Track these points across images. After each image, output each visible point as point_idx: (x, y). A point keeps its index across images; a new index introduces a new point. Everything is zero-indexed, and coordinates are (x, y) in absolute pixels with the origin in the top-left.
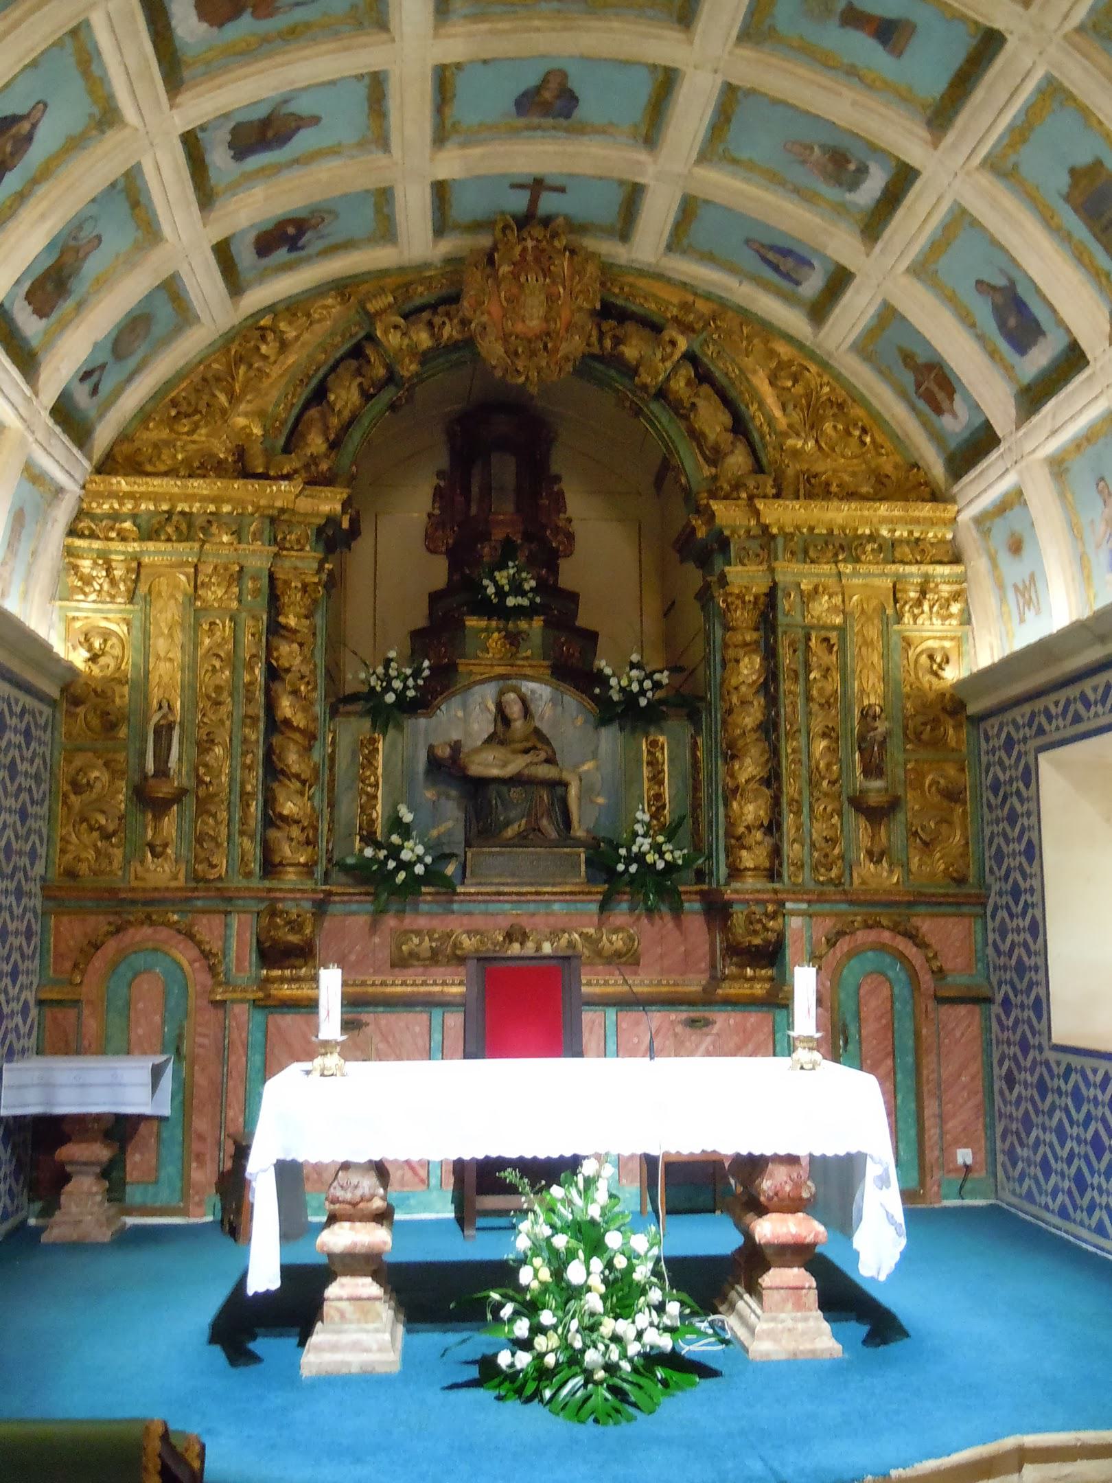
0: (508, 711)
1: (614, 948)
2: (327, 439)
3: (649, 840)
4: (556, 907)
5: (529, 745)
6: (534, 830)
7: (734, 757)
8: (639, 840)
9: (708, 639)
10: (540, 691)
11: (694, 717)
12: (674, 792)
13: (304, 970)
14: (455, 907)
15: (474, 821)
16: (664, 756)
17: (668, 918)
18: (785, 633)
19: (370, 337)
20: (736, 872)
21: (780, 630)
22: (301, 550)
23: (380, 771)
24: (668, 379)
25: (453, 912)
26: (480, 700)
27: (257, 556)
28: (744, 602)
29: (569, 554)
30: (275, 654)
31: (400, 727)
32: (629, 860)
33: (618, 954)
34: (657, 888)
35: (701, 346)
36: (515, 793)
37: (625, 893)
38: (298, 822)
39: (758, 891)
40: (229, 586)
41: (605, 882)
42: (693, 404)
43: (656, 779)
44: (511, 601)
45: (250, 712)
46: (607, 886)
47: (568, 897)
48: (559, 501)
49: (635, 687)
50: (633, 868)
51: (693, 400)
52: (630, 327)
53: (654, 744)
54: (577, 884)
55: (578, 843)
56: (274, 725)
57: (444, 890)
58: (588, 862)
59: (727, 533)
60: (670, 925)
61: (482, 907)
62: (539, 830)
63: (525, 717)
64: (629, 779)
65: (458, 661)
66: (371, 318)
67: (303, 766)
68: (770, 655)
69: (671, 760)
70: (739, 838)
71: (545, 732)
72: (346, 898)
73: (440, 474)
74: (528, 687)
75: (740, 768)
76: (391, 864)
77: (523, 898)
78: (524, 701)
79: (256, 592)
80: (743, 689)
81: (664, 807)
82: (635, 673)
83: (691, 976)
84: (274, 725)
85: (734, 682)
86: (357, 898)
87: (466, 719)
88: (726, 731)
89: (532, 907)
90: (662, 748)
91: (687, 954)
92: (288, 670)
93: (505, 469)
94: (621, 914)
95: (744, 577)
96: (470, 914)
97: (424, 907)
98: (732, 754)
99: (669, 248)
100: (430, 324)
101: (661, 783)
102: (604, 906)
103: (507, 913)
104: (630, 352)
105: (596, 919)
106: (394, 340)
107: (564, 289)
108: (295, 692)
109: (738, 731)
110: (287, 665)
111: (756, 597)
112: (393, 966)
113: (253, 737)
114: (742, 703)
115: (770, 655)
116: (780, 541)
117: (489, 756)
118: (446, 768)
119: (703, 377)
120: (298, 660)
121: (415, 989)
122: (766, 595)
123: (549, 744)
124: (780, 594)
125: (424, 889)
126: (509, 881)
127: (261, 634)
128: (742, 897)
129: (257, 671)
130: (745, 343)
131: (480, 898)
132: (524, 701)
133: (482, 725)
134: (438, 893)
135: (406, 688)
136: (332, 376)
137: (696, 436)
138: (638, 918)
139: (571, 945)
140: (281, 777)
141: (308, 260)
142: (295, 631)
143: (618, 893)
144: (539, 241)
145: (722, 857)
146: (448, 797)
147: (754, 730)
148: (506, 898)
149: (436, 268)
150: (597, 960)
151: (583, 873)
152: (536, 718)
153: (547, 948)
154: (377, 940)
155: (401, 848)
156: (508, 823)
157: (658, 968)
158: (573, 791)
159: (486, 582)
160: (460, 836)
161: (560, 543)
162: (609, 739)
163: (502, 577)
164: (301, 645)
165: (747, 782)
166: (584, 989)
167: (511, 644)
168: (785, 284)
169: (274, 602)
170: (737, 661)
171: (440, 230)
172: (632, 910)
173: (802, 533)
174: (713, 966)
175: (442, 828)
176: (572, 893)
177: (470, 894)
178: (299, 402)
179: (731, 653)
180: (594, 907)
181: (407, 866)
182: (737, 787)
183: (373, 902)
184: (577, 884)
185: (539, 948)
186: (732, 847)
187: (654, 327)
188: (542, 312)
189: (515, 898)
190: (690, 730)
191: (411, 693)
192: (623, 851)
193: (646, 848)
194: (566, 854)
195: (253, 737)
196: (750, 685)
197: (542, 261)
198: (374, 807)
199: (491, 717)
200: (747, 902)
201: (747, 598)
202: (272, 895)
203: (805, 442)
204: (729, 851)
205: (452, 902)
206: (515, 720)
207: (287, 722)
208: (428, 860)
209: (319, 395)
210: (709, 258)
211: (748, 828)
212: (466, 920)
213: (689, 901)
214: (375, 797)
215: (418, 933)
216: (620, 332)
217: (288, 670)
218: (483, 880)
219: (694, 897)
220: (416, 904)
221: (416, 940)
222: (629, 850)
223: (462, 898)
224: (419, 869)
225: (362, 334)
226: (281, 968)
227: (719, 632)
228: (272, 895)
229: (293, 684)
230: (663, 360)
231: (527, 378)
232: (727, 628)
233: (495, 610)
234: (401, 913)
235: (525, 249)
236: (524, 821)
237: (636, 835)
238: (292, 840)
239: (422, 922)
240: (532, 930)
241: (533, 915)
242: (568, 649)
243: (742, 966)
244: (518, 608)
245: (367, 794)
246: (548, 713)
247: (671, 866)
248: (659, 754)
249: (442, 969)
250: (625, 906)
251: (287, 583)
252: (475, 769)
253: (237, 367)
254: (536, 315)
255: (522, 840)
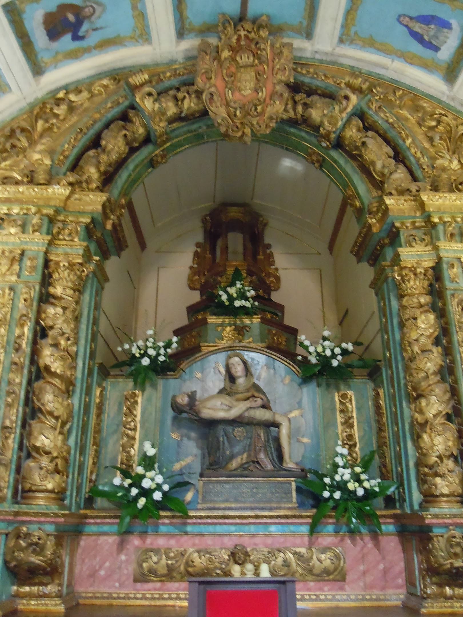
0: (233, 371)
1: (323, 566)
2: (99, 171)
3: (349, 471)
4: (273, 528)
5: (250, 394)
6: (254, 462)
7: (420, 396)
8: (340, 470)
9: (383, 312)
10: (258, 359)
11: (373, 372)
12: (362, 434)
13: (49, 587)
14: (189, 529)
15: (207, 455)
16: (353, 407)
17: (367, 539)
18: (453, 295)
19: (133, 107)
20: (430, 498)
21: (448, 293)
22: (72, 240)
23: (138, 418)
24: (344, 126)
25: (186, 533)
26: (213, 365)
27: (36, 242)
28: (415, 274)
29: (277, 289)
30: (43, 316)
31: (154, 386)
32: (333, 488)
33: (327, 572)
34: (357, 512)
35: (367, 104)
36: (238, 432)
37: (330, 517)
38: (48, 453)
39: (455, 516)
40: (12, 265)
41: (313, 507)
42: (364, 143)
43: (348, 423)
44: (237, 303)
45: (16, 360)
46: (315, 510)
47: (282, 521)
48: (270, 259)
49: (328, 353)
50: (337, 495)
51: (364, 140)
52: (315, 98)
53: (344, 396)
54: (289, 509)
55: (289, 473)
56: (38, 373)
57: (178, 514)
58: (299, 490)
59: (397, 224)
60: (370, 545)
61: (211, 528)
62: (258, 463)
63: (246, 376)
64: (329, 424)
65: (201, 344)
66: (134, 89)
67: (57, 405)
68: (442, 314)
69: (358, 409)
70: (431, 467)
71: (262, 387)
72: (98, 521)
73: (198, 245)
74: (248, 356)
75: (427, 405)
76: (134, 491)
77: (245, 521)
78: (245, 362)
79: (33, 268)
80: (423, 340)
81: (355, 445)
82: (327, 343)
83: (390, 591)
84: (38, 373)
85: (414, 336)
86: (108, 520)
87: (205, 381)
88: (411, 375)
89: (252, 528)
90: (351, 400)
91: (386, 571)
92: (51, 328)
93: (236, 241)
94: (327, 536)
95: (414, 255)
96: (201, 535)
97: (163, 529)
98: (417, 396)
99: (341, 41)
100: (176, 98)
101: (351, 426)
102: (313, 529)
103: (232, 535)
104: (315, 115)
105: (306, 539)
106: (148, 105)
107: (268, 66)
108: (56, 345)
109: (423, 374)
110: (51, 324)
111: (426, 270)
112: (136, 581)
113: (17, 380)
114: (423, 351)
115: (442, 314)
116: (440, 228)
117: (218, 403)
118: (187, 414)
119: (368, 127)
120: (60, 321)
121: (153, 603)
122: (433, 268)
123: (264, 393)
124: (445, 266)
125: (162, 513)
126: (233, 505)
127: (32, 300)
128: (441, 521)
129: (26, 329)
130: (398, 102)
131: (209, 521)
132: (245, 362)
133: (215, 381)
134: (173, 517)
135: (158, 354)
136: (106, 131)
137: (366, 169)
138: (342, 540)
139: (286, 564)
140: (40, 415)
141: (88, 50)
142: (59, 298)
143: (325, 517)
144: (249, 32)
145: (414, 484)
146: (189, 438)
147: (435, 373)
148: (231, 521)
149: (180, 64)
150: (310, 577)
151: (294, 500)
152: (255, 377)
153: (265, 573)
154: (123, 557)
155: (143, 477)
156: (232, 457)
157: (361, 584)
158: (284, 431)
159: (221, 293)
160: (198, 469)
161: (272, 282)
162: (310, 394)
163: (232, 291)
164: (64, 309)
165: (435, 416)
166: (300, 605)
167: (239, 334)
168: (427, 53)
169: (46, 280)
170: (415, 319)
171: (181, 34)
172: (337, 532)
173: (456, 222)
174: (410, 582)
175: (183, 463)
176: (286, 517)
177: (201, 517)
178: (80, 145)
179: (409, 313)
180: (305, 529)
181: (146, 493)
182: (426, 422)
183: (118, 524)
184: (289, 509)
185: (257, 573)
186: (425, 475)
187: (330, 96)
188: (252, 85)
189: (238, 521)
190: (370, 386)
191: (162, 358)
192: (327, 480)
193: (347, 477)
194: (280, 482)
195: (17, 380)
196: (429, 337)
197: (253, 46)
198: (132, 446)
199: (222, 378)
200: (446, 526)
201: (419, 270)
202: (20, 518)
203: (451, 162)
204: (422, 480)
205: (185, 524)
206: (239, 377)
207: (47, 368)
208: (166, 487)
209: (96, 143)
210: (370, 43)
211: (440, 457)
212: (197, 540)
213: (385, 523)
214: (134, 438)
215: (157, 551)
216: (308, 101)
217: (51, 328)
218: (217, 505)
219: (389, 520)
220: (157, 525)
221: (155, 559)
222: (333, 479)
223: (194, 520)
224: (157, 496)
225: (127, 103)
226: (31, 585)
227: (395, 304)
228: (20, 518)
229: (55, 338)
230: (341, 112)
231: (243, 133)
232: (401, 296)
233: (229, 310)
234: (143, 534)
235: (240, 36)
236: (245, 455)
237: (336, 466)
238: (41, 468)
239: (161, 542)
240: (253, 549)
241: (254, 536)
242: (278, 339)
243: (440, 585)
244: (243, 307)
245: (128, 435)
246: (264, 374)
247: (369, 494)
248: (348, 405)
249: (176, 585)
250: (330, 528)
251: (57, 263)
252: (207, 413)
253: (36, 121)
254: (248, 88)
255: (244, 471)
